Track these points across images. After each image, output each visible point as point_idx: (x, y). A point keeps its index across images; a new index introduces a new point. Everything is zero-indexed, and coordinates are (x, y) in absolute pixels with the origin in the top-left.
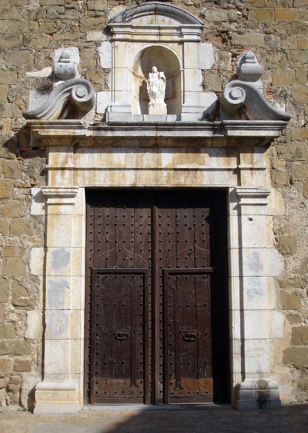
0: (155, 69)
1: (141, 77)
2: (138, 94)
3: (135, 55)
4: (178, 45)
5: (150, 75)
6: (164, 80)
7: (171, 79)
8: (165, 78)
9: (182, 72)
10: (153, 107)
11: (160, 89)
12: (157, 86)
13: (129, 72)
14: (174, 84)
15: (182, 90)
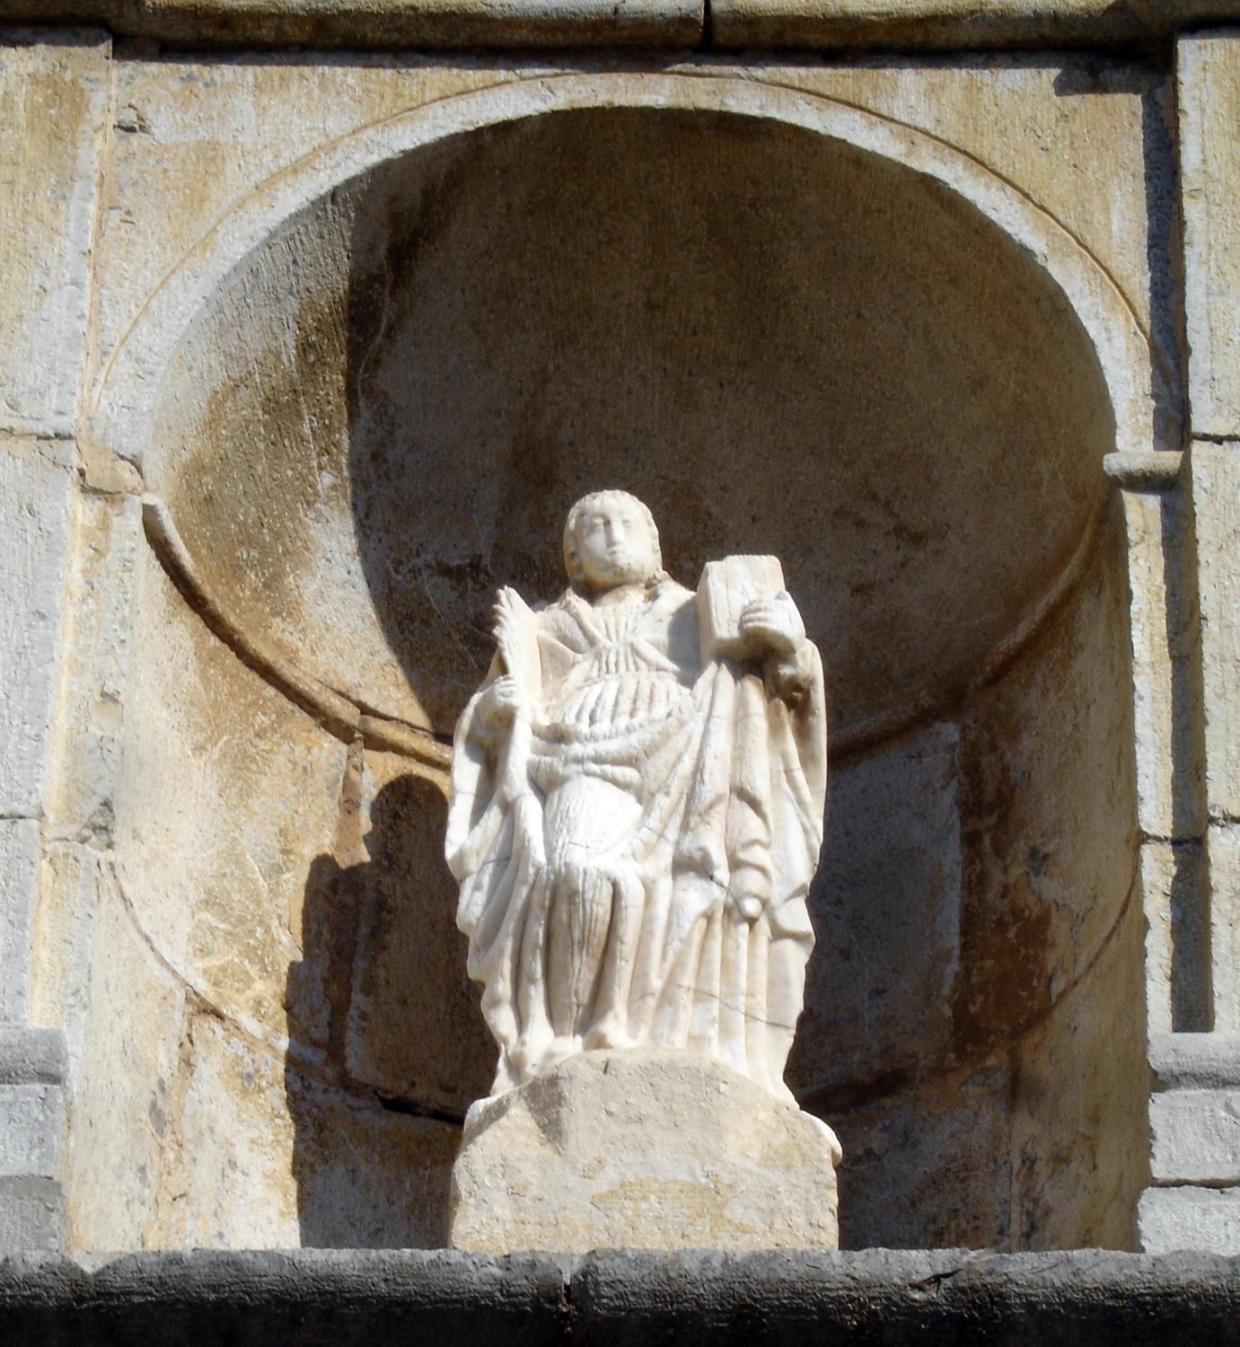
0: (624, 525)
1: (348, 714)
2: (269, 989)
3: (236, 244)
4: (1062, 88)
5: (519, 623)
6: (792, 697)
7: (950, 732)
8: (809, 662)
9: (1141, 513)
10: (552, 1130)
11: (712, 842)
12: (644, 796)
13: (84, 512)
14: (992, 808)
15: (1156, 813)
